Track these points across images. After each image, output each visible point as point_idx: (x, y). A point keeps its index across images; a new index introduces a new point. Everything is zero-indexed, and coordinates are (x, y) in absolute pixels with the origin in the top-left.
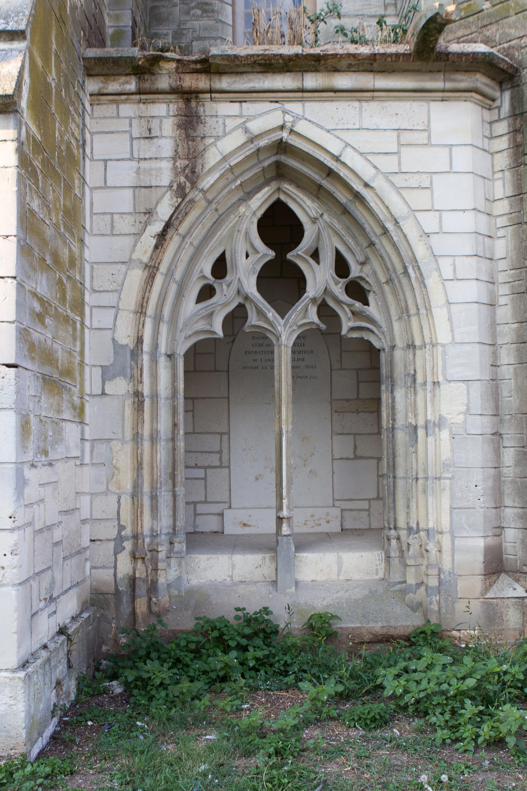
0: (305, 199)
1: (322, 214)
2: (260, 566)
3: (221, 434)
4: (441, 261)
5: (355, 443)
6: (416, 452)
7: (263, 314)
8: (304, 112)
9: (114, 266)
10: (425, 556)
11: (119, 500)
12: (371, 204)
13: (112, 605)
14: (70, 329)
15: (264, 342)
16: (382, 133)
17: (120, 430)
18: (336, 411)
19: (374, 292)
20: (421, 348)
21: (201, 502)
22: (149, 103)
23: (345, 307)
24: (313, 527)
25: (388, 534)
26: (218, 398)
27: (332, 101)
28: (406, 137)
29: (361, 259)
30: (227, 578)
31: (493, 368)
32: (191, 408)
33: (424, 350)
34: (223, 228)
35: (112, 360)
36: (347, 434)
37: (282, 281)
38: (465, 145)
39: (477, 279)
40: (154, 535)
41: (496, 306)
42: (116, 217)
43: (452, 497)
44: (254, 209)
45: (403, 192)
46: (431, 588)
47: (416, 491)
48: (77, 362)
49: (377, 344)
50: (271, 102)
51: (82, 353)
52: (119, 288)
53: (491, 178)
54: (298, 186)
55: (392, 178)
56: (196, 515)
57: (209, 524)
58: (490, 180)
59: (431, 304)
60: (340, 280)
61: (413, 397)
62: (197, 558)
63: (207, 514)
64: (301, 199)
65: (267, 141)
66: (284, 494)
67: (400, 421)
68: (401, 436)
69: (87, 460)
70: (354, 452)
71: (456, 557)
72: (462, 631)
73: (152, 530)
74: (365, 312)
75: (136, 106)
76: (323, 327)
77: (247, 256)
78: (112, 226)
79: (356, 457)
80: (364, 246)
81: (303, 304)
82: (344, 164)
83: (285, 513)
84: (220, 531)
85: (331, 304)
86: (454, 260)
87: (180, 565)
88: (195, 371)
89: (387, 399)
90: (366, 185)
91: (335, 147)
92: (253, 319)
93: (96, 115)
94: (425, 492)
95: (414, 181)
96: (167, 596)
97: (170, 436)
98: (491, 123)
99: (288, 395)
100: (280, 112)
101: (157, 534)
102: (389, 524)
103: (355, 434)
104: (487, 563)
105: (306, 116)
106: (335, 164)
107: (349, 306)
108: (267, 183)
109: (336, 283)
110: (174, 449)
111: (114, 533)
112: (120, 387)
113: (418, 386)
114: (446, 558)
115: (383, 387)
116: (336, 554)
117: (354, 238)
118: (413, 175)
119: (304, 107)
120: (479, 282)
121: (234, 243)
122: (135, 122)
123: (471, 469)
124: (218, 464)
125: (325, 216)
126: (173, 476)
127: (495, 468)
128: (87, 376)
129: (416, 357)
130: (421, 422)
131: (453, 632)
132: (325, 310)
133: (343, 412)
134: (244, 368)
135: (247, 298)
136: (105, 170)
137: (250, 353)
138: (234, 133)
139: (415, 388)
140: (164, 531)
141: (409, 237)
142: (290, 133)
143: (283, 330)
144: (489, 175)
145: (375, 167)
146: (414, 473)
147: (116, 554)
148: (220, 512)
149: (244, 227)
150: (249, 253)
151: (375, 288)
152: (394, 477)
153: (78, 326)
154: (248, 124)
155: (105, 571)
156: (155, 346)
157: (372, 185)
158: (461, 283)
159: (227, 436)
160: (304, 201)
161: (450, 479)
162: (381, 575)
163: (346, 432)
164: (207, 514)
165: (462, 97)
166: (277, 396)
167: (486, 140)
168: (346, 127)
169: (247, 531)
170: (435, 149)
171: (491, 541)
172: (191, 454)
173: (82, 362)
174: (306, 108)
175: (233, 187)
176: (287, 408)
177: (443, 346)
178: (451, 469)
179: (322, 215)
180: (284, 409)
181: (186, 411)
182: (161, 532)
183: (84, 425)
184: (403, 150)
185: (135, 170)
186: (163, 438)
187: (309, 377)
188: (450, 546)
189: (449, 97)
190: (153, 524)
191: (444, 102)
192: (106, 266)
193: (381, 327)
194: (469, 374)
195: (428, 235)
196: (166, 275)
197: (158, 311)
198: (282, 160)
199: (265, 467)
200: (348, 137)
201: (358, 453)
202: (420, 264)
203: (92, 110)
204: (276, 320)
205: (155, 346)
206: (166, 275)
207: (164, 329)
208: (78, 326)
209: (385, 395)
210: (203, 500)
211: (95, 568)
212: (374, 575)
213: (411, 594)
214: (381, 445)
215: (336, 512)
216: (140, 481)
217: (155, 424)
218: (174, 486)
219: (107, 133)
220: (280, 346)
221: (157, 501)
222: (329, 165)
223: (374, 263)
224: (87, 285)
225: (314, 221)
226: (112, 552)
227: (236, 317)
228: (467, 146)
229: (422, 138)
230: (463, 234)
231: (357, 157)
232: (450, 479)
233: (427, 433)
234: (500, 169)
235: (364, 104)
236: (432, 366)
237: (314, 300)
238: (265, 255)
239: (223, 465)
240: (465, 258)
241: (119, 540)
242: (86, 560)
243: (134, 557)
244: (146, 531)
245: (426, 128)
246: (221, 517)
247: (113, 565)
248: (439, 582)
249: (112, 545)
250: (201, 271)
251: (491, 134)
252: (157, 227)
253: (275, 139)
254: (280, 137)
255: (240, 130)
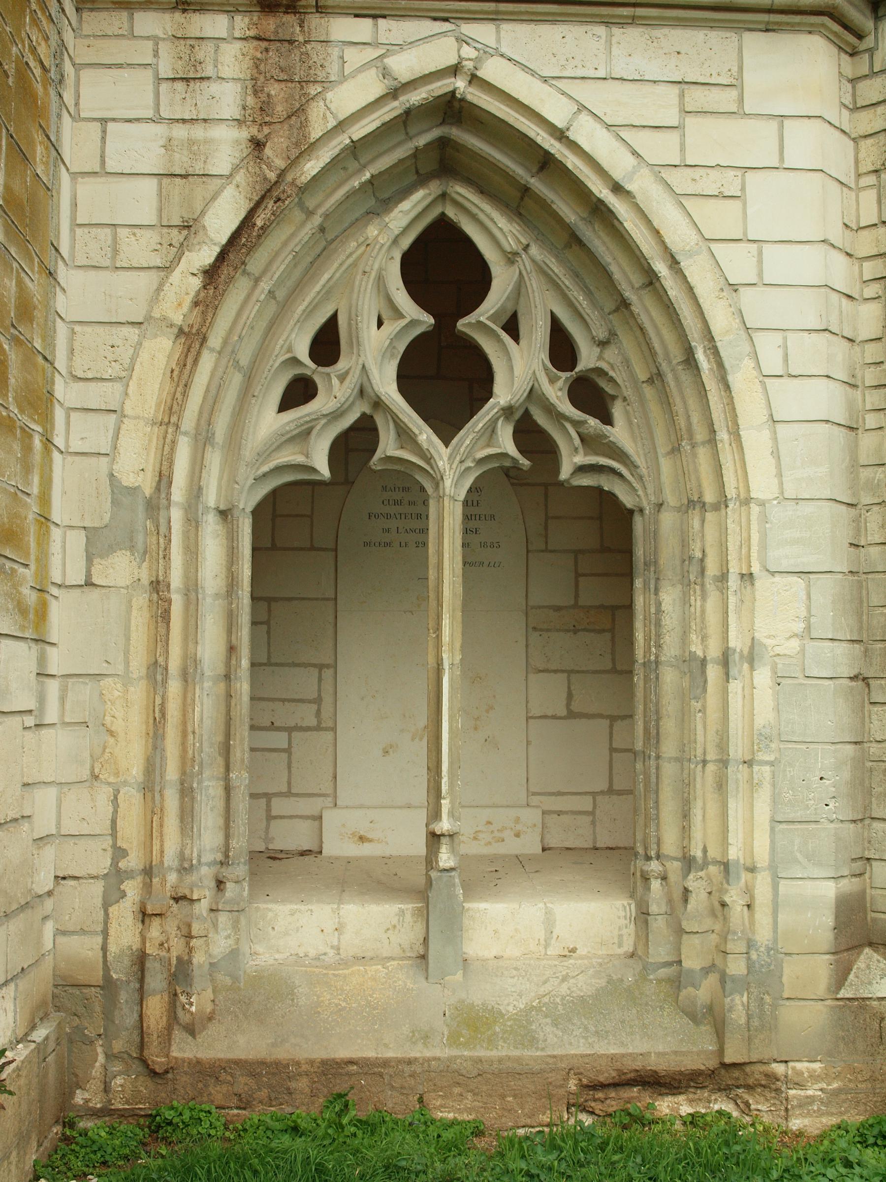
0: (496, 215)
1: (528, 245)
2: (395, 927)
3: (321, 667)
4: (758, 337)
5: (569, 688)
6: (703, 710)
7: (409, 434)
8: (498, 41)
9: (114, 330)
10: (719, 914)
11: (116, 798)
12: (625, 224)
13: (98, 1009)
14: (17, 447)
15: (408, 491)
16: (648, 87)
17: (121, 657)
18: (535, 629)
19: (625, 399)
20: (716, 507)
21: (279, 794)
22: (195, 11)
23: (568, 426)
24: (490, 843)
25: (645, 868)
26: (317, 599)
27: (554, 22)
28: (697, 98)
29: (601, 333)
30: (328, 950)
31: (852, 549)
32: (264, 617)
33: (723, 511)
34: (336, 265)
35: (107, 518)
36: (556, 671)
37: (444, 375)
38: (809, 117)
39: (828, 377)
40: (186, 867)
41: (860, 431)
42: (122, 233)
43: (775, 800)
44: (397, 232)
45: (688, 203)
46: (734, 979)
47: (703, 785)
48: (31, 516)
49: (627, 500)
50: (435, 19)
51: (45, 499)
52: (124, 374)
53: (853, 185)
54: (482, 191)
55: (666, 174)
56: (270, 818)
57: (292, 836)
58: (850, 188)
59: (740, 422)
60: (560, 374)
61: (699, 603)
62: (270, 910)
63: (291, 817)
64: (488, 216)
65: (424, 95)
66: (444, 788)
67: (671, 648)
68: (669, 677)
69: (51, 716)
70: (568, 705)
71: (781, 917)
72: (791, 1064)
73: (182, 857)
74: (606, 437)
75: (167, 16)
76: (524, 462)
77: (380, 324)
78: (115, 252)
79: (572, 715)
80: (607, 310)
81: (487, 418)
82: (574, 146)
83: (444, 825)
84: (315, 848)
85: (541, 419)
86: (785, 339)
87: (236, 926)
88: (274, 547)
89: (647, 607)
90: (617, 188)
91: (556, 111)
92: (388, 445)
93: (86, 30)
94: (721, 785)
95: (709, 183)
96: (210, 990)
97: (221, 670)
98: (853, 81)
99: (454, 594)
100: (453, 39)
101: (192, 865)
102: (646, 849)
103: (570, 672)
104: (839, 928)
105: (504, 50)
106: (557, 145)
107: (576, 424)
108: (422, 180)
109: (552, 380)
110: (229, 696)
111: (104, 864)
112: (121, 569)
113: (708, 581)
114: (763, 917)
115: (638, 583)
116: (541, 905)
117: (589, 294)
118: (709, 171)
119: (498, 32)
120: (831, 382)
121: (355, 296)
122: (163, 48)
123: (812, 746)
124: (313, 722)
125: (534, 250)
126: (226, 750)
127: (856, 743)
128: (55, 547)
129: (706, 525)
130: (714, 651)
131: (774, 1065)
132: (528, 433)
133: (548, 630)
134: (366, 544)
135: (378, 404)
136: (103, 139)
137: (377, 516)
138: (361, 77)
139: (703, 585)
140: (207, 858)
141: (699, 291)
142: (470, 82)
143: (447, 467)
144: (851, 181)
145: (635, 153)
146: (699, 752)
147: (106, 906)
148: (316, 814)
149: (376, 267)
150: (384, 317)
151: (628, 392)
152: (658, 757)
153: (37, 442)
154: (390, 61)
155: (86, 939)
156: (196, 491)
157: (628, 187)
158: (796, 381)
159: (331, 671)
160: (492, 220)
161: (771, 764)
162: (628, 947)
163: (553, 667)
164: (291, 817)
165: (805, 24)
166: (432, 595)
167: (845, 112)
168: (580, 73)
169: (366, 850)
170: (751, 122)
171: (848, 885)
172: (264, 704)
173: (44, 520)
174: (503, 33)
175: (356, 184)
176: (453, 618)
177: (762, 504)
178: (773, 745)
179: (526, 248)
180: (446, 622)
181: (254, 623)
182: (199, 861)
183: (48, 648)
184: (690, 121)
185: (162, 142)
186: (208, 673)
187: (486, 563)
188: (769, 896)
189: (777, 23)
190: (183, 846)
191: (770, 34)
192: (100, 329)
193: (636, 467)
194: (809, 562)
195: (734, 288)
196: (220, 353)
197: (203, 422)
198: (449, 136)
199: (402, 731)
200: (584, 93)
201: (575, 707)
202: (719, 344)
203: (80, 20)
204: (434, 447)
205: (196, 491)
206: (220, 353)
207: (214, 460)
208: (37, 442)
209: (641, 599)
210: (284, 789)
211: (64, 933)
212: (615, 946)
213: (690, 989)
214: (631, 696)
215: (532, 816)
216: (158, 760)
217: (191, 646)
218: (228, 769)
219: (109, 66)
220: (440, 498)
221: (193, 799)
222: (546, 146)
223: (625, 342)
224: (61, 362)
225: (511, 258)
226: (99, 901)
227: (356, 443)
228: (812, 120)
229: (725, 100)
230: (801, 289)
231: (601, 133)
232: (771, 764)
233: (727, 674)
234: (872, 168)
235: (616, 30)
236: (738, 543)
237: (507, 411)
238: (413, 323)
239: (323, 725)
240: (806, 334)
241: (116, 877)
242: (45, 918)
243: (144, 916)
244: (170, 857)
245: (734, 82)
246: (317, 823)
247: (100, 928)
248: (748, 968)
249: (98, 888)
250: (290, 350)
251: (855, 102)
252: (206, 256)
253: (440, 92)
254: (451, 89)
255: (373, 71)
